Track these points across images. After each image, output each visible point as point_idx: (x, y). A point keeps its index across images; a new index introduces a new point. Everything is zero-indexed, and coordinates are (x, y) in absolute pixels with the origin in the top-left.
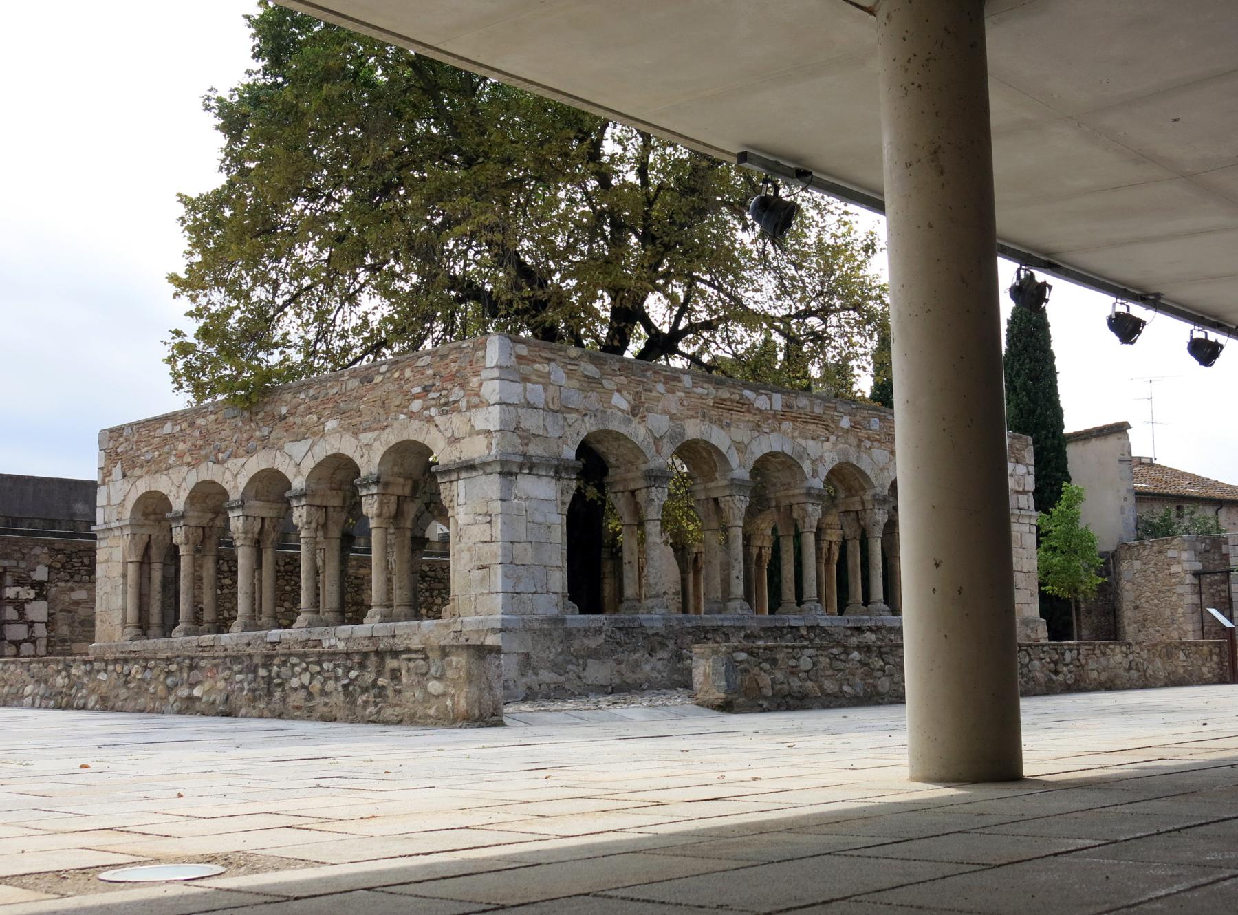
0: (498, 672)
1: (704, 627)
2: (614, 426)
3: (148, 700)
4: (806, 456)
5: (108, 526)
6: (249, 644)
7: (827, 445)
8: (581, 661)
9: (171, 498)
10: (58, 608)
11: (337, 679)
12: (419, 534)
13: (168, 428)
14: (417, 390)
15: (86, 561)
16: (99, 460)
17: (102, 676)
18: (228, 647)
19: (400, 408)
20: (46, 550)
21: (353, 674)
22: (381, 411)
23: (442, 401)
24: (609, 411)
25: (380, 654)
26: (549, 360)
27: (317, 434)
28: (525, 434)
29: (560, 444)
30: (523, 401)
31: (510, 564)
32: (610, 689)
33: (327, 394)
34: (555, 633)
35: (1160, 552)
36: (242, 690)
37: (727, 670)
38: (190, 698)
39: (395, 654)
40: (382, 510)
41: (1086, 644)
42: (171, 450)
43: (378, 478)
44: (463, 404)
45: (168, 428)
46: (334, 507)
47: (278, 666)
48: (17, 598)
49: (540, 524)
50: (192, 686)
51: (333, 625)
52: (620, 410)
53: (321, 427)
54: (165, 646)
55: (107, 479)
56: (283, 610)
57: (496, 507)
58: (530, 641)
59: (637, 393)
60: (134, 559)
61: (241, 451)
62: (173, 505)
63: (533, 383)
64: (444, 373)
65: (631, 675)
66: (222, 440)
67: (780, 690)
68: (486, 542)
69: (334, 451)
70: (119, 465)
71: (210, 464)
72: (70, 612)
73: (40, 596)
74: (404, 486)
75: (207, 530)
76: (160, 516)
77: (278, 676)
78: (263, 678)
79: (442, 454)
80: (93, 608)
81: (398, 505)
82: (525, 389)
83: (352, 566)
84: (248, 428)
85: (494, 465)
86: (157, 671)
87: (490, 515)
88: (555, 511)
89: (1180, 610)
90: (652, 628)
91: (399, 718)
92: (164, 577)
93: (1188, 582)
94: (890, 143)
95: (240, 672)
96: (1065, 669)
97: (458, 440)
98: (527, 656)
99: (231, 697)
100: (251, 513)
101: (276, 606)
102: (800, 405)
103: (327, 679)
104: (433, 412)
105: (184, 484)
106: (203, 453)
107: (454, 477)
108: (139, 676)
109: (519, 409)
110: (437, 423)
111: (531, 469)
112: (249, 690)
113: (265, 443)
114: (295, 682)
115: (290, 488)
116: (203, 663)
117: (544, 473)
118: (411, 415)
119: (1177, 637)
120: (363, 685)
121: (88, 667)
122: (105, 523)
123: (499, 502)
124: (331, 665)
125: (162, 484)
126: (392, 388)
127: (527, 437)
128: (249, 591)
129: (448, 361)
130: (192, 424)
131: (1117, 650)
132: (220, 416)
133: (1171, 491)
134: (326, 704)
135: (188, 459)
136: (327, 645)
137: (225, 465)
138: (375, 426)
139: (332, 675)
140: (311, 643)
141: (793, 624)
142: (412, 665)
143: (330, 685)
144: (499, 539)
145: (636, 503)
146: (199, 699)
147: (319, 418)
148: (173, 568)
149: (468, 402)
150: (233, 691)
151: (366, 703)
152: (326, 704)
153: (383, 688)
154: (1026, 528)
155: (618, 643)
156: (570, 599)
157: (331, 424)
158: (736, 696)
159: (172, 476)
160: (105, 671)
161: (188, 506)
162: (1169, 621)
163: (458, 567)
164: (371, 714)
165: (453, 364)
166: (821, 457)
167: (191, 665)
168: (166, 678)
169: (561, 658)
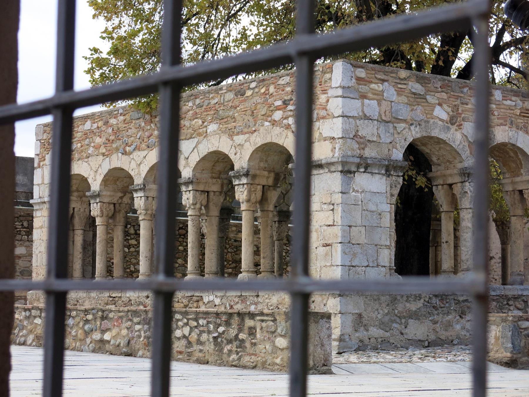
2: (435, 133)
3: (71, 340)
8: (403, 321)
9: (90, 181)
11: (209, 332)
12: (285, 209)
14: (279, 103)
15: (25, 224)
16: (36, 148)
18: (131, 298)
21: (221, 329)
22: (251, 119)
24: (432, 121)
26: (383, 81)
27: (202, 135)
28: (362, 140)
29: (391, 148)
30: (361, 114)
32: (426, 344)
33: (209, 103)
36: (139, 337)
37: (513, 335)
38: (102, 341)
39: (252, 316)
42: (90, 143)
43: (248, 171)
46: (214, 192)
49: (373, 212)
50: (103, 332)
52: (441, 120)
53: (205, 129)
55: (42, 163)
57: (338, 198)
59: (455, 106)
61: (143, 146)
63: (369, 100)
65: (444, 332)
66: (129, 136)
68: (329, 226)
69: (215, 149)
71: (120, 155)
74: (268, 178)
75: (117, 206)
80: (30, 261)
82: (363, 104)
83: (233, 231)
84: (149, 127)
85: (336, 165)
86: (77, 319)
88: (385, 202)
91: (254, 364)
92: (84, 241)
95: (139, 323)
98: (360, 316)
99: (132, 342)
103: (202, 332)
105: (100, 169)
106: (114, 146)
109: (357, 121)
111: (366, 168)
112: (145, 337)
116: (111, 315)
117: (377, 172)
118: (274, 123)
120: (228, 338)
121: (28, 313)
122: (40, 198)
123: (340, 194)
124: (205, 322)
128: (148, 255)
130: (106, 123)
132: (127, 117)
134: (201, 351)
135: (103, 150)
136: (207, 300)
137: (131, 156)
138: (246, 130)
139: (206, 329)
140: (195, 299)
142: (264, 325)
143: (204, 337)
144: (340, 223)
145: (453, 195)
146: (108, 342)
147: (203, 122)
148: (91, 233)
150: (134, 337)
151: (230, 351)
152: (201, 351)
153: (243, 341)
155: (434, 307)
156: (396, 271)
157: (212, 127)
158: (520, 356)
159: (91, 163)
161: (103, 187)
164: (234, 360)
167: (103, 316)
168: (84, 325)
169: (387, 319)
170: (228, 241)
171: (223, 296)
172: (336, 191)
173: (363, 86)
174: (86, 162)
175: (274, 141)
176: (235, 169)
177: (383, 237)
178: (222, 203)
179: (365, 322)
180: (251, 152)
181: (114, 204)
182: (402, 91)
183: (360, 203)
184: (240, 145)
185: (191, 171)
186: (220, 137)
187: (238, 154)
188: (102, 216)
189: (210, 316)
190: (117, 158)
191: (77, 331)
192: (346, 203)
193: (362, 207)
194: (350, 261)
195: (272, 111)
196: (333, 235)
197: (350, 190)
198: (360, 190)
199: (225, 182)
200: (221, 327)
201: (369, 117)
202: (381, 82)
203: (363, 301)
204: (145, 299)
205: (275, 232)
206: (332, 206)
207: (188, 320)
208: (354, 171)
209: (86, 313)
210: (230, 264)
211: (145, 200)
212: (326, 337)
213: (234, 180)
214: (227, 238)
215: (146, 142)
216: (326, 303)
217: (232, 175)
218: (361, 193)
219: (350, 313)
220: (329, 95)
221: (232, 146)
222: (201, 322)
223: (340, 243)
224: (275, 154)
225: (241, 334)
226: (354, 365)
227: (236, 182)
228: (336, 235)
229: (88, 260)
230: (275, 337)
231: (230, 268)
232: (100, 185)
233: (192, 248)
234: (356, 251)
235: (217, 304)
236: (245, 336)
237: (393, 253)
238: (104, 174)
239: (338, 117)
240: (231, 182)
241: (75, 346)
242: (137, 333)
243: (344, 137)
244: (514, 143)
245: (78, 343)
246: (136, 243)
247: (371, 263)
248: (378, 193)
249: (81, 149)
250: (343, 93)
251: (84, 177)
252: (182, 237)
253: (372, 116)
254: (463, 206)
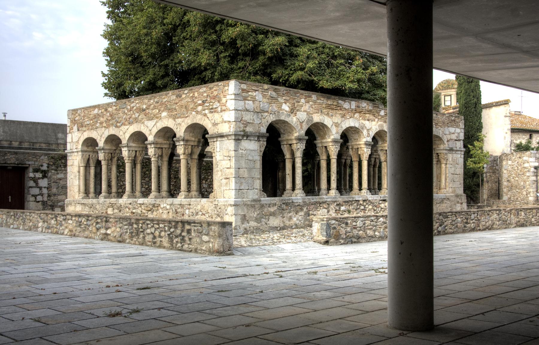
0: (231, 233)
1: (319, 202)
2: (283, 118)
4: (365, 128)
5: (72, 151)
6: (130, 204)
7: (374, 123)
8: (267, 217)
9: (98, 141)
10: (52, 181)
11: (165, 231)
13: (96, 111)
14: (200, 102)
17: (70, 222)
19: (193, 109)
20: (46, 157)
21: (172, 230)
23: (211, 107)
25: (183, 223)
26: (256, 91)
29: (260, 126)
30: (244, 108)
31: (238, 177)
33: (162, 101)
34: (257, 206)
35: (520, 158)
37: (326, 228)
38: (106, 234)
39: (189, 223)
40: (185, 151)
41: (480, 211)
43: (184, 138)
44: (219, 109)
45: (96, 111)
47: (142, 224)
48: (35, 177)
49: (251, 160)
50: (107, 229)
51: (165, 198)
53: (160, 115)
54: (96, 202)
55: (71, 131)
56: (145, 181)
57: (233, 153)
60: (83, 165)
62: (99, 144)
63: (249, 101)
64: (211, 95)
67: (349, 235)
69: (165, 126)
70: (76, 125)
71: (114, 127)
72: (57, 183)
73: (44, 177)
75: (113, 154)
77: (142, 227)
78: (136, 228)
79: (211, 130)
81: (192, 149)
82: (245, 103)
84: (129, 113)
86: (93, 221)
89: (527, 183)
90: (297, 203)
91: (190, 250)
93: (532, 171)
94: (390, 65)
95: (126, 225)
96: (471, 222)
97: (217, 124)
98: (245, 216)
100: (131, 149)
102: (363, 106)
104: (207, 112)
105: (103, 135)
107: (215, 140)
108: (85, 223)
109: (242, 112)
110: (208, 116)
111: (247, 137)
112: (130, 233)
113: (136, 120)
114: (149, 231)
116: (111, 220)
118: (197, 112)
119: (525, 194)
121: (64, 217)
122: (71, 149)
123: (234, 152)
125: (94, 134)
126: (189, 100)
127: (247, 124)
129: (213, 90)
130: (106, 110)
131: (494, 213)
132: (118, 107)
133: (526, 128)
135: (105, 125)
137: (120, 128)
138: (182, 116)
141: (357, 199)
142: (196, 228)
143: (163, 234)
144: (234, 167)
146: (110, 235)
149: (221, 108)
151: (177, 242)
153: (184, 237)
154: (459, 156)
156: (263, 191)
157: (164, 114)
159: (98, 132)
160: (71, 219)
162: (522, 187)
163: (216, 178)
165: (215, 92)
166: (371, 128)
169: (259, 216)
177: (256, 174)
179: (248, 219)
181: (111, 153)
184: (179, 124)
191: (92, 228)
207: (154, 224)
218: (245, 150)
220: (227, 98)
222: (161, 225)
227: (177, 144)
235: (168, 208)
237: (261, 182)
242: (125, 230)
244: (323, 122)
246: (123, 170)
254: (297, 156)
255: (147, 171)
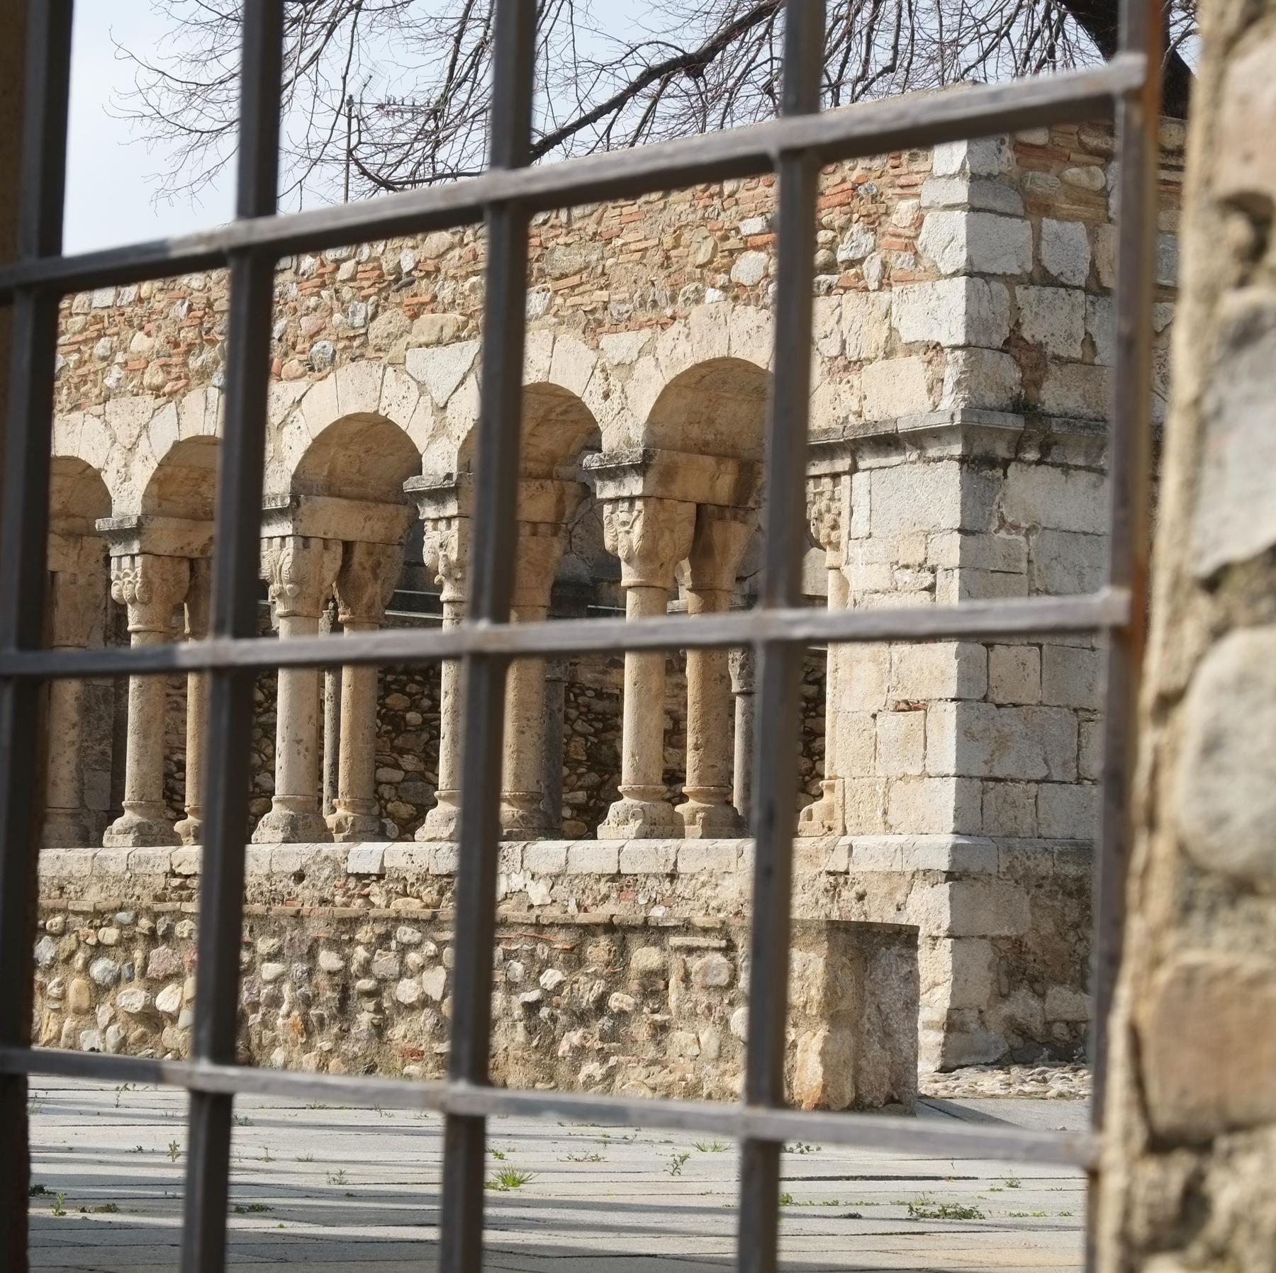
6: (300, 877)
9: (109, 479)
21: (551, 977)
30: (1029, 267)
36: (275, 1001)
39: (654, 932)
42: (113, 352)
44: (872, 270)
47: (368, 946)
50: (155, 985)
56: (398, 776)
58: (1026, 908)
76: (78, 522)
77: (366, 969)
86: (68, 942)
87: (933, 570)
95: (273, 957)
100: (316, 528)
101: (378, 764)
105: (143, 442)
107: (843, 464)
109: (1019, 290)
111: (1045, 449)
114: (407, 991)
115: (417, 469)
117: (1081, 461)
135: (154, 376)
142: (695, 964)
151: (580, 1052)
159: (115, 422)
167: (153, 931)
170: (576, 696)
171: (558, 876)
172: (943, 526)
173: (1038, 174)
174: (99, 417)
175: (739, 355)
176: (605, 446)
178: (559, 562)
180: (660, 389)
182: (1170, 193)
183: (1024, 565)
185: (456, 451)
186: (555, 339)
187: (615, 396)
188: (150, 600)
189: (513, 935)
190: (203, 406)
192: (978, 565)
193: (1031, 580)
194: (986, 762)
195: (731, 252)
196: (931, 673)
197: (989, 523)
198: (1023, 525)
199: (572, 488)
200: (549, 972)
201: (1056, 278)
202: (1100, 161)
203: (1028, 898)
204: (291, 883)
205: (737, 664)
206: (928, 574)
208: (1004, 459)
209: (97, 922)
210: (580, 776)
211: (296, 548)
212: (899, 1005)
213: (599, 484)
214: (572, 685)
215: (303, 353)
216: (904, 903)
217: (595, 466)
218: (1028, 532)
219: (984, 937)
220: (925, 203)
221: (594, 368)
223: (953, 700)
224: (740, 398)
225: (615, 995)
226: (990, 1101)
228: (942, 672)
229: (98, 748)
230: (731, 1003)
231: (581, 788)
232: (144, 496)
233: (455, 712)
234: (1006, 729)
236: (632, 1001)
238: (159, 459)
239: (954, 274)
240: (587, 492)
241: (60, 1032)
243: (973, 343)
245: (68, 1021)
247: (1059, 769)
248: (1085, 533)
249: (80, 371)
250: (971, 194)
251: (90, 466)
252: (418, 678)
253: (1069, 274)
255: (414, 706)
